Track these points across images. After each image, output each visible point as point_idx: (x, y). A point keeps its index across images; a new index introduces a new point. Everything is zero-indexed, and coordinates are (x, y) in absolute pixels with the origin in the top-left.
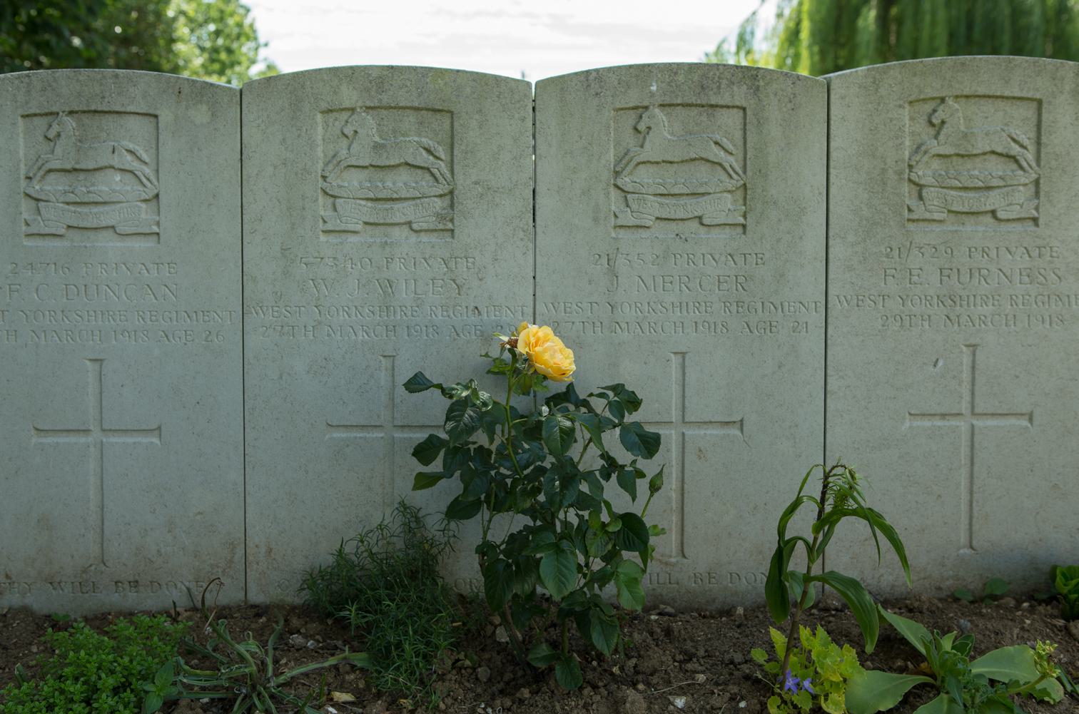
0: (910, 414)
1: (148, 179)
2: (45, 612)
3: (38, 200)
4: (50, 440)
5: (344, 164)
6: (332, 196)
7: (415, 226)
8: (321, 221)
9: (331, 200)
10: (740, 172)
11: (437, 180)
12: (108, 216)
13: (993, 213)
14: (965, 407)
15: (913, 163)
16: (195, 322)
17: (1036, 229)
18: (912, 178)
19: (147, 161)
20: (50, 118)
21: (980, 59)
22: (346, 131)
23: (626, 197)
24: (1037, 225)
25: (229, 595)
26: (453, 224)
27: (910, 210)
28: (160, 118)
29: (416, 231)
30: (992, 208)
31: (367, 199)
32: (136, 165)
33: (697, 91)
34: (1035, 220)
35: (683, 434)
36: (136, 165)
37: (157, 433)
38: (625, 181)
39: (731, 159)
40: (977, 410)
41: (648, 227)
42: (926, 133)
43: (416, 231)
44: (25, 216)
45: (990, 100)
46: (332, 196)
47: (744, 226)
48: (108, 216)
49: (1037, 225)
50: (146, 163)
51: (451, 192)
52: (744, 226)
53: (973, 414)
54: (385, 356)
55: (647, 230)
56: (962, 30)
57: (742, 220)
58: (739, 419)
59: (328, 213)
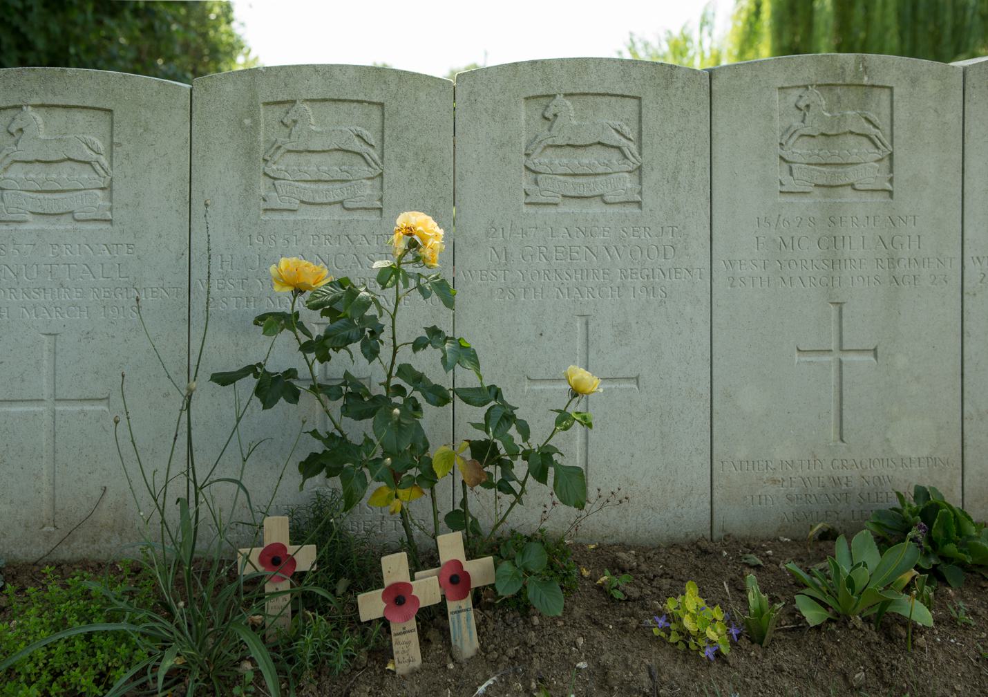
0: (799, 350)
3: (275, 179)
5: (544, 144)
6: (534, 172)
7: (77, 216)
8: (524, 194)
9: (532, 176)
10: (379, 162)
11: (626, 157)
12: (851, 175)
14: (833, 345)
15: (783, 142)
17: (890, 200)
18: (529, 166)
19: (373, 143)
21: (807, 57)
22: (547, 115)
23: (791, 167)
25: (79, 549)
28: (115, 114)
29: (348, 209)
30: (341, 199)
31: (565, 175)
32: (363, 148)
33: (640, 89)
34: (639, 203)
35: (841, 362)
36: (363, 148)
37: (106, 401)
39: (371, 151)
40: (845, 348)
41: (809, 193)
42: (541, 128)
43: (348, 209)
44: (524, 185)
45: (85, 110)
46: (534, 172)
48: (851, 175)
49: (112, 224)
51: (381, 175)
52: (381, 209)
53: (841, 350)
54: (318, 324)
55: (808, 195)
56: (908, 10)
58: (873, 348)
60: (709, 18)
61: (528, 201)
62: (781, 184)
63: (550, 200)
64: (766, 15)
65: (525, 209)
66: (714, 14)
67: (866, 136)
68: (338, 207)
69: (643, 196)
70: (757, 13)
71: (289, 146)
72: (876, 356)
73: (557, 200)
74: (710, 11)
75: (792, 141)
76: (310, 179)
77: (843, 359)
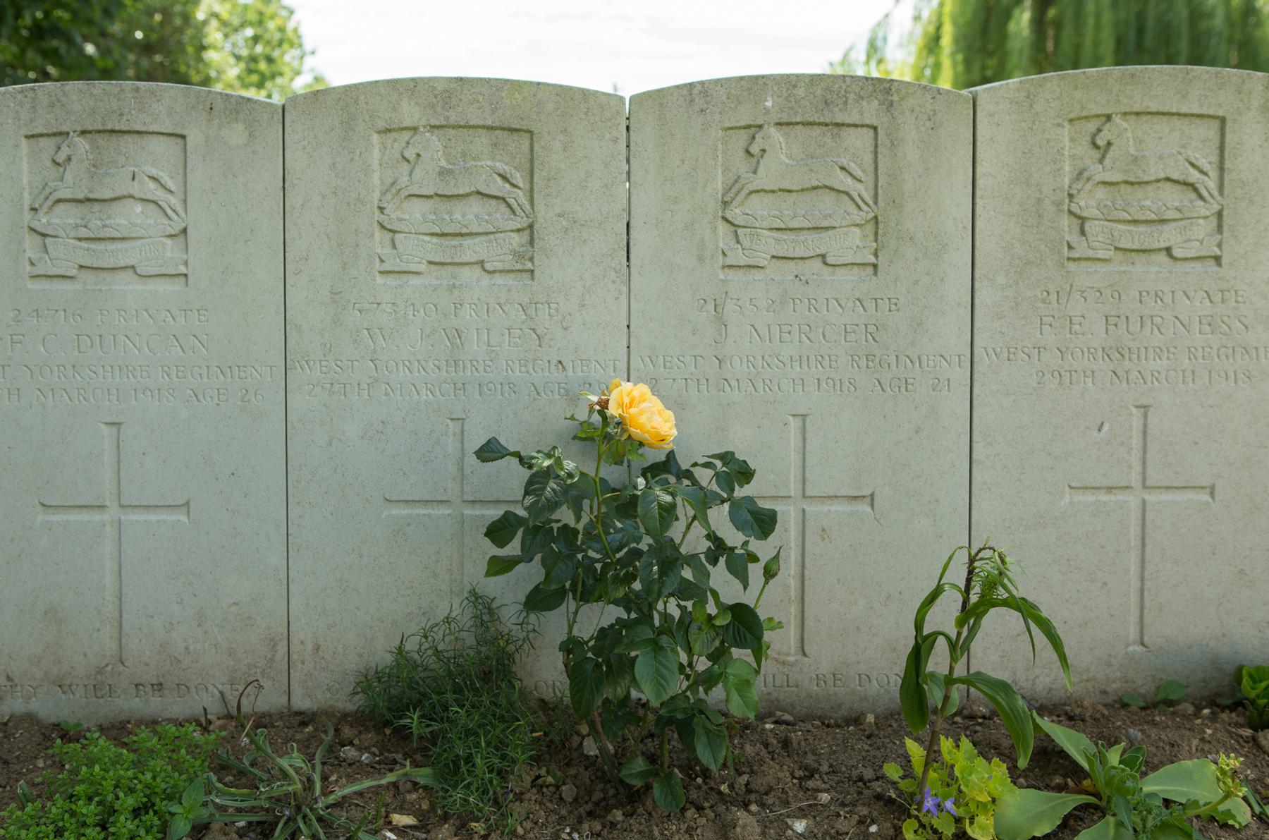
0: (1071, 487)
3: (44, 235)
5: (404, 193)
6: (391, 231)
7: (488, 266)
9: (388, 235)
10: (871, 203)
13: (1168, 250)
14: (1135, 479)
15: (1075, 192)
20: (59, 139)
22: (407, 155)
24: (1219, 265)
29: (489, 272)
32: (159, 194)
35: (804, 511)
36: (159, 194)
38: (735, 213)
39: (860, 187)
40: (1149, 483)
44: (29, 254)
46: (391, 231)
47: (875, 266)
51: (531, 226)
53: (1145, 487)
56: (1132, 35)
59: (386, 251)
60: (879, 43)
61: (382, 269)
62: (1070, 247)
63: (412, 267)
64: (947, 41)
65: (380, 280)
66: (885, 39)
67: (155, 202)
68: (477, 269)
69: (536, 263)
70: (936, 38)
71: (756, 185)
72: (1212, 494)
73: (73, 272)
74: (880, 34)
75: (739, 199)
76: (783, 226)
77: (807, 509)
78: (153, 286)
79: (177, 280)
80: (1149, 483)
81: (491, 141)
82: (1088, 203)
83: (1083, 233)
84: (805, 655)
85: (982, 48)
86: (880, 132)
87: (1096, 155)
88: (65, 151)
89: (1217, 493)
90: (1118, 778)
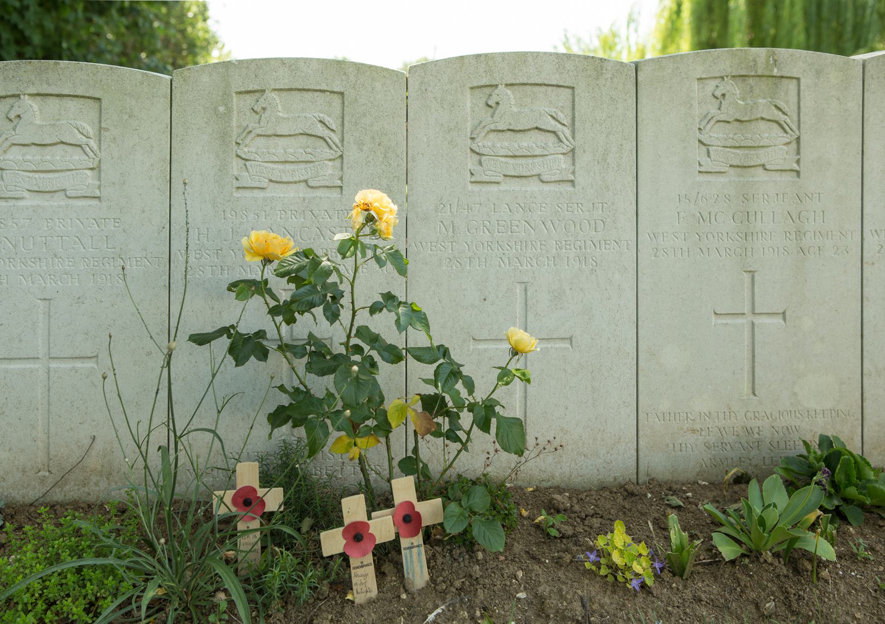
0: (715, 313)
1: (336, 146)
2: (668, 476)
3: (246, 160)
4: (482, 346)
6: (478, 154)
7: (68, 193)
9: (477, 157)
10: (340, 145)
12: (763, 157)
13: (763, 166)
14: (747, 309)
16: (598, 250)
17: (797, 179)
20: (488, 91)
24: (574, 186)
25: (71, 492)
26: (799, 165)
27: (700, 165)
28: (103, 101)
29: (312, 187)
30: (305, 178)
32: (325, 133)
36: (325, 133)
37: (95, 359)
38: (244, 151)
46: (478, 154)
47: (341, 187)
48: (763, 157)
50: (564, 125)
51: (341, 156)
52: (341, 187)
56: (814, 9)
57: (339, 183)
59: (476, 168)
61: (473, 180)
63: (493, 179)
65: (470, 187)
70: (678, 12)
71: (259, 131)
72: (784, 319)
78: (319, 193)
79: (334, 189)
80: (756, 311)
81: (335, 95)
82: (484, 143)
83: (480, 163)
84: (754, 394)
85: (712, 24)
86: (802, 81)
87: (716, 103)
88: (262, 103)
89: (787, 317)
90: (557, 474)
